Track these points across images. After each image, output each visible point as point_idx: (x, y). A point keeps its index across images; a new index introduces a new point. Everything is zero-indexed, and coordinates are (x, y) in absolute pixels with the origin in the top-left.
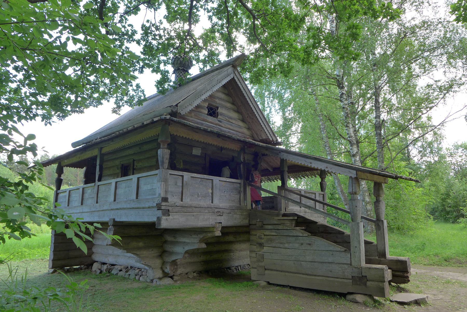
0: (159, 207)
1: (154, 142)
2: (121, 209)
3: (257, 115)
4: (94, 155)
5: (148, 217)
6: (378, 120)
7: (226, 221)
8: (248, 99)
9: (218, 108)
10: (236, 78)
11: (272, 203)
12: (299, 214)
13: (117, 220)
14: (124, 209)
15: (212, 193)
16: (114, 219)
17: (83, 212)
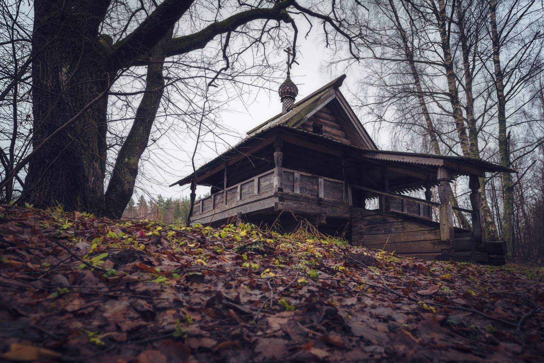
1: (270, 149)
2: (246, 204)
3: (359, 131)
4: (221, 169)
6: (503, 134)
8: (350, 117)
10: (337, 98)
17: (215, 214)
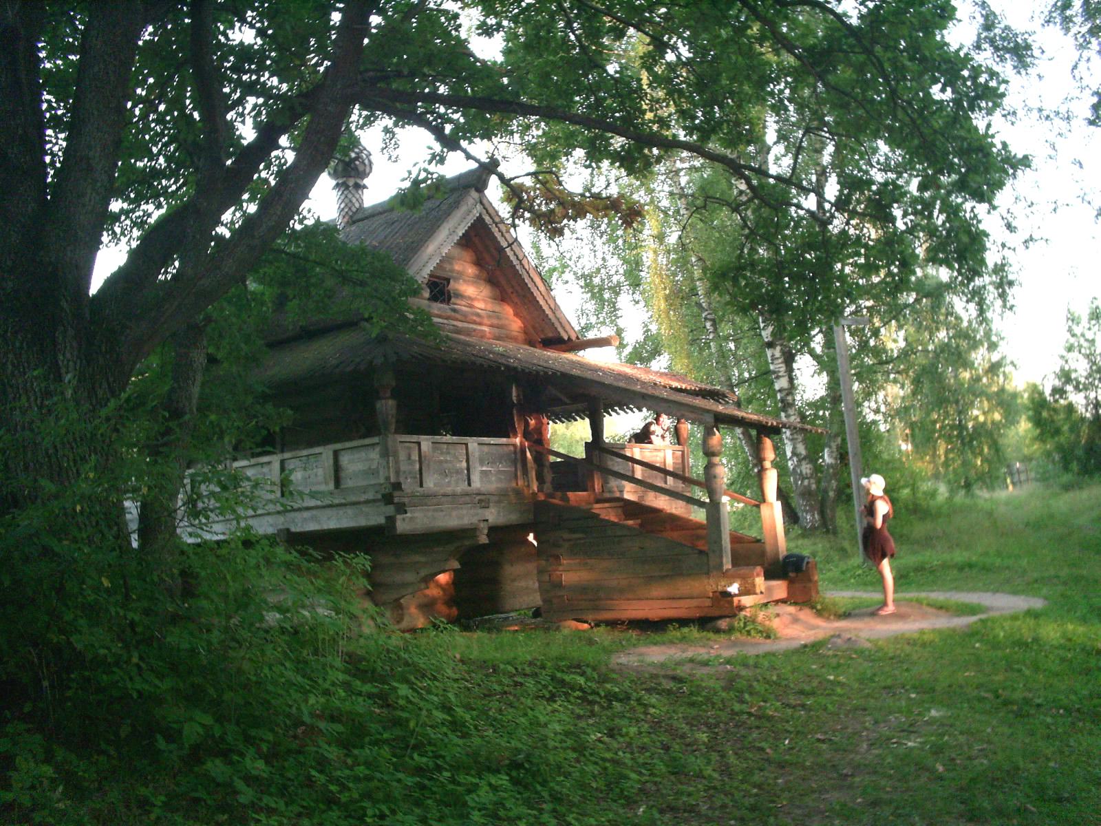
0: (388, 499)
5: (374, 517)
7: (494, 516)
9: (448, 281)
10: (487, 219)
11: (571, 473)
12: (615, 384)
13: (293, 529)
14: (308, 509)
15: (421, 469)
16: (288, 530)
